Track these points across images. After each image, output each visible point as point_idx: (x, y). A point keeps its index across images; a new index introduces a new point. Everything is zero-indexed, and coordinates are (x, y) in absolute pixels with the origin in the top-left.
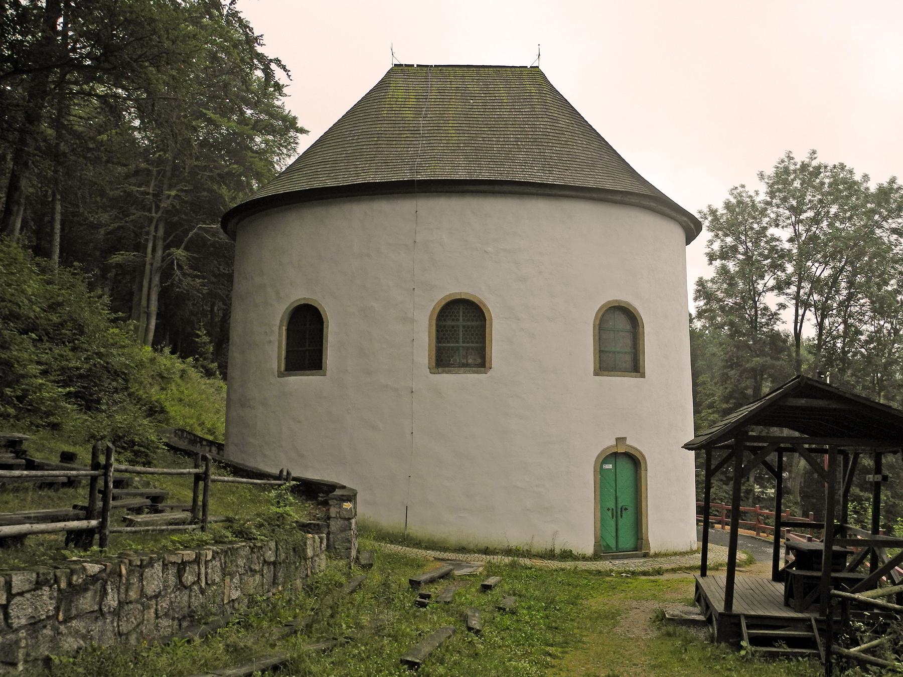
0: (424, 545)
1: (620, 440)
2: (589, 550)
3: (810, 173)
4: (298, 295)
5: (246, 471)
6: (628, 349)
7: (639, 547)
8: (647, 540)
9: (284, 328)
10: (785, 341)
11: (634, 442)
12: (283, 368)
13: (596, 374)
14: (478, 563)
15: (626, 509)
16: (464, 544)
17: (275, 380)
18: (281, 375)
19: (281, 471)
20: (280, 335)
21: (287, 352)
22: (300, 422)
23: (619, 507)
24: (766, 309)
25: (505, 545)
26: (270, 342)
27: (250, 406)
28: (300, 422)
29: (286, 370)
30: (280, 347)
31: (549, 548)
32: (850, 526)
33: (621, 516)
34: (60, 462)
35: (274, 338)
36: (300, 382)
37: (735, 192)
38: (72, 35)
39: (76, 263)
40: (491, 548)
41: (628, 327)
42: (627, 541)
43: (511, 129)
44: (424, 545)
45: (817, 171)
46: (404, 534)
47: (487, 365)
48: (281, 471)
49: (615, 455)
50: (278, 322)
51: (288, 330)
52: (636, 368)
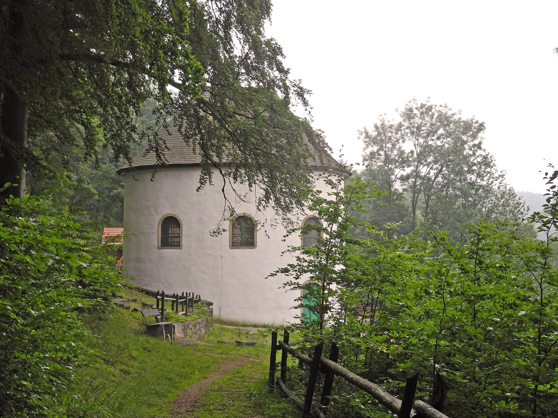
0: (228, 324)
3: (426, 110)
4: (167, 211)
5: (152, 293)
9: (160, 227)
10: (407, 210)
14: (253, 330)
16: (245, 323)
17: (156, 251)
18: (159, 248)
19: (183, 294)
20: (158, 230)
21: (161, 238)
22: (169, 270)
24: (332, 284)
25: (263, 324)
26: (153, 233)
27: (142, 262)
28: (169, 270)
29: (161, 246)
30: (158, 236)
31: (281, 325)
35: (155, 231)
36: (167, 252)
37: (381, 118)
39: (496, 366)
40: (257, 325)
44: (228, 324)
45: (430, 108)
46: (219, 319)
47: (255, 245)
48: (183, 294)
50: (157, 224)
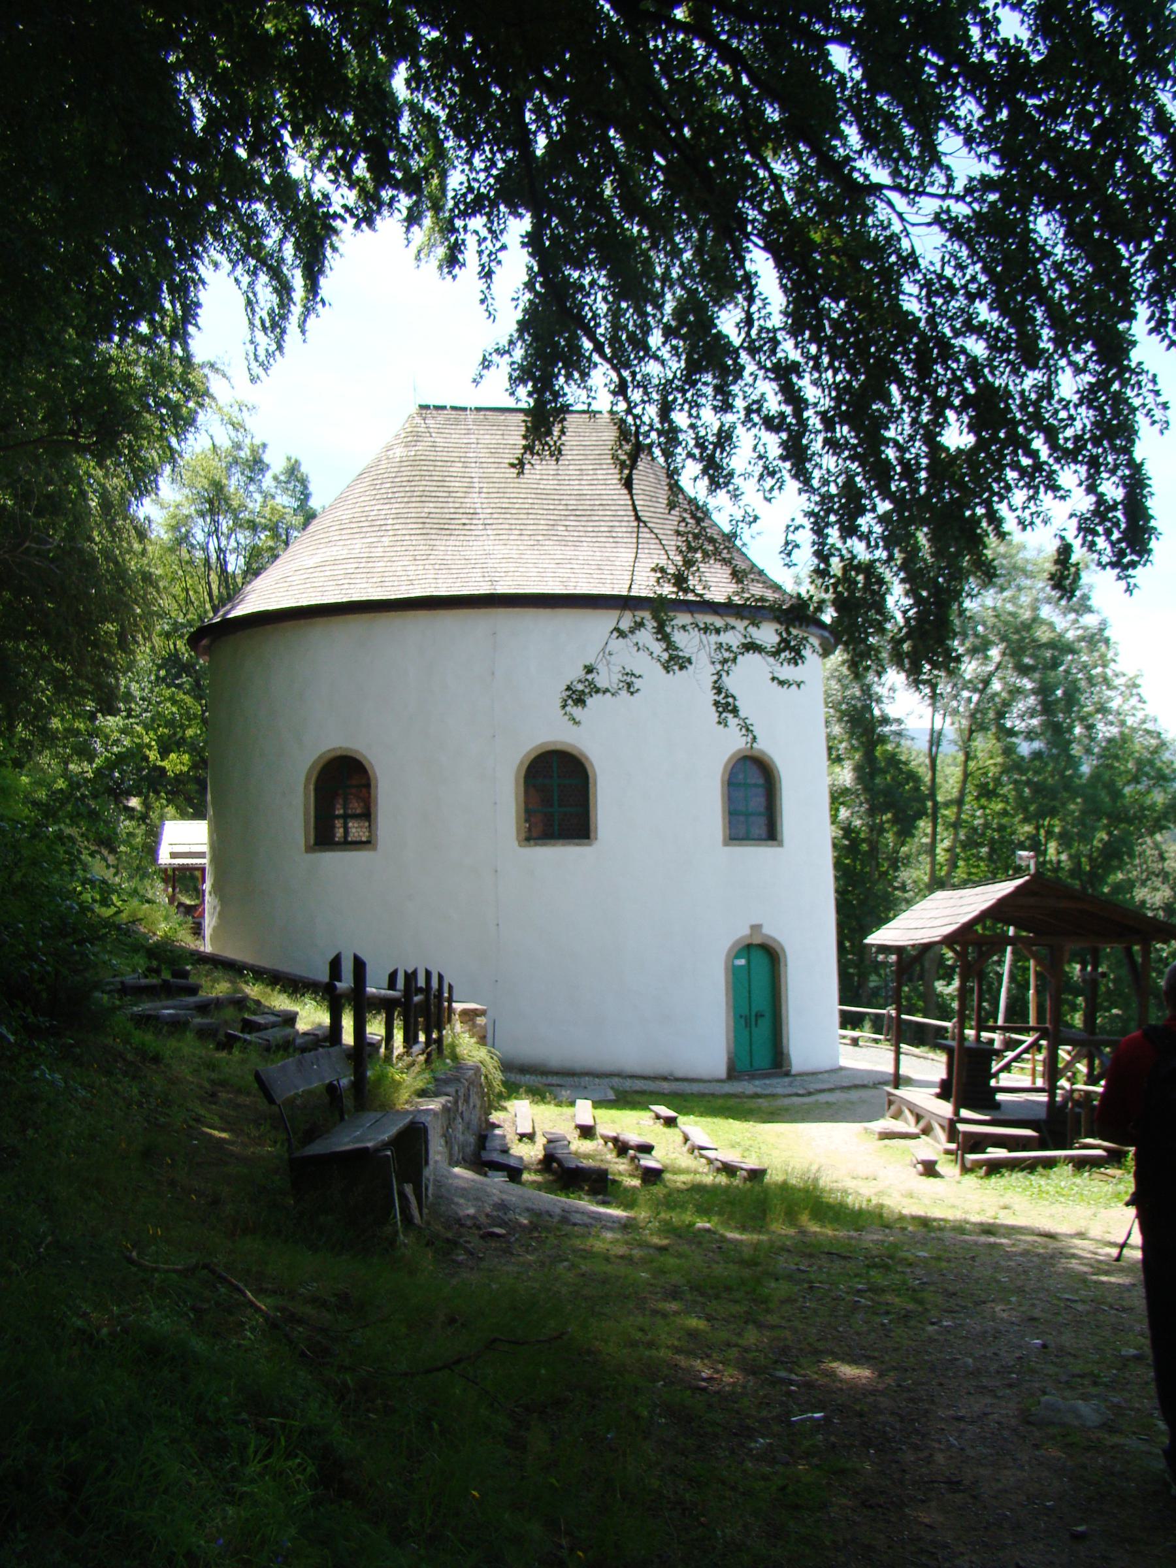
1: (756, 928)
2: (721, 1070)
6: (762, 809)
7: (778, 1061)
8: (788, 1055)
9: (312, 787)
11: (774, 931)
12: (312, 841)
13: (726, 844)
15: (762, 1016)
23: (753, 1014)
32: (249, 453)
33: (756, 1024)
34: (296, 1014)
38: (984, 1009)
41: (761, 781)
42: (763, 1059)
43: (601, 513)
47: (592, 835)
49: (749, 947)
51: (316, 789)
52: (771, 834)
